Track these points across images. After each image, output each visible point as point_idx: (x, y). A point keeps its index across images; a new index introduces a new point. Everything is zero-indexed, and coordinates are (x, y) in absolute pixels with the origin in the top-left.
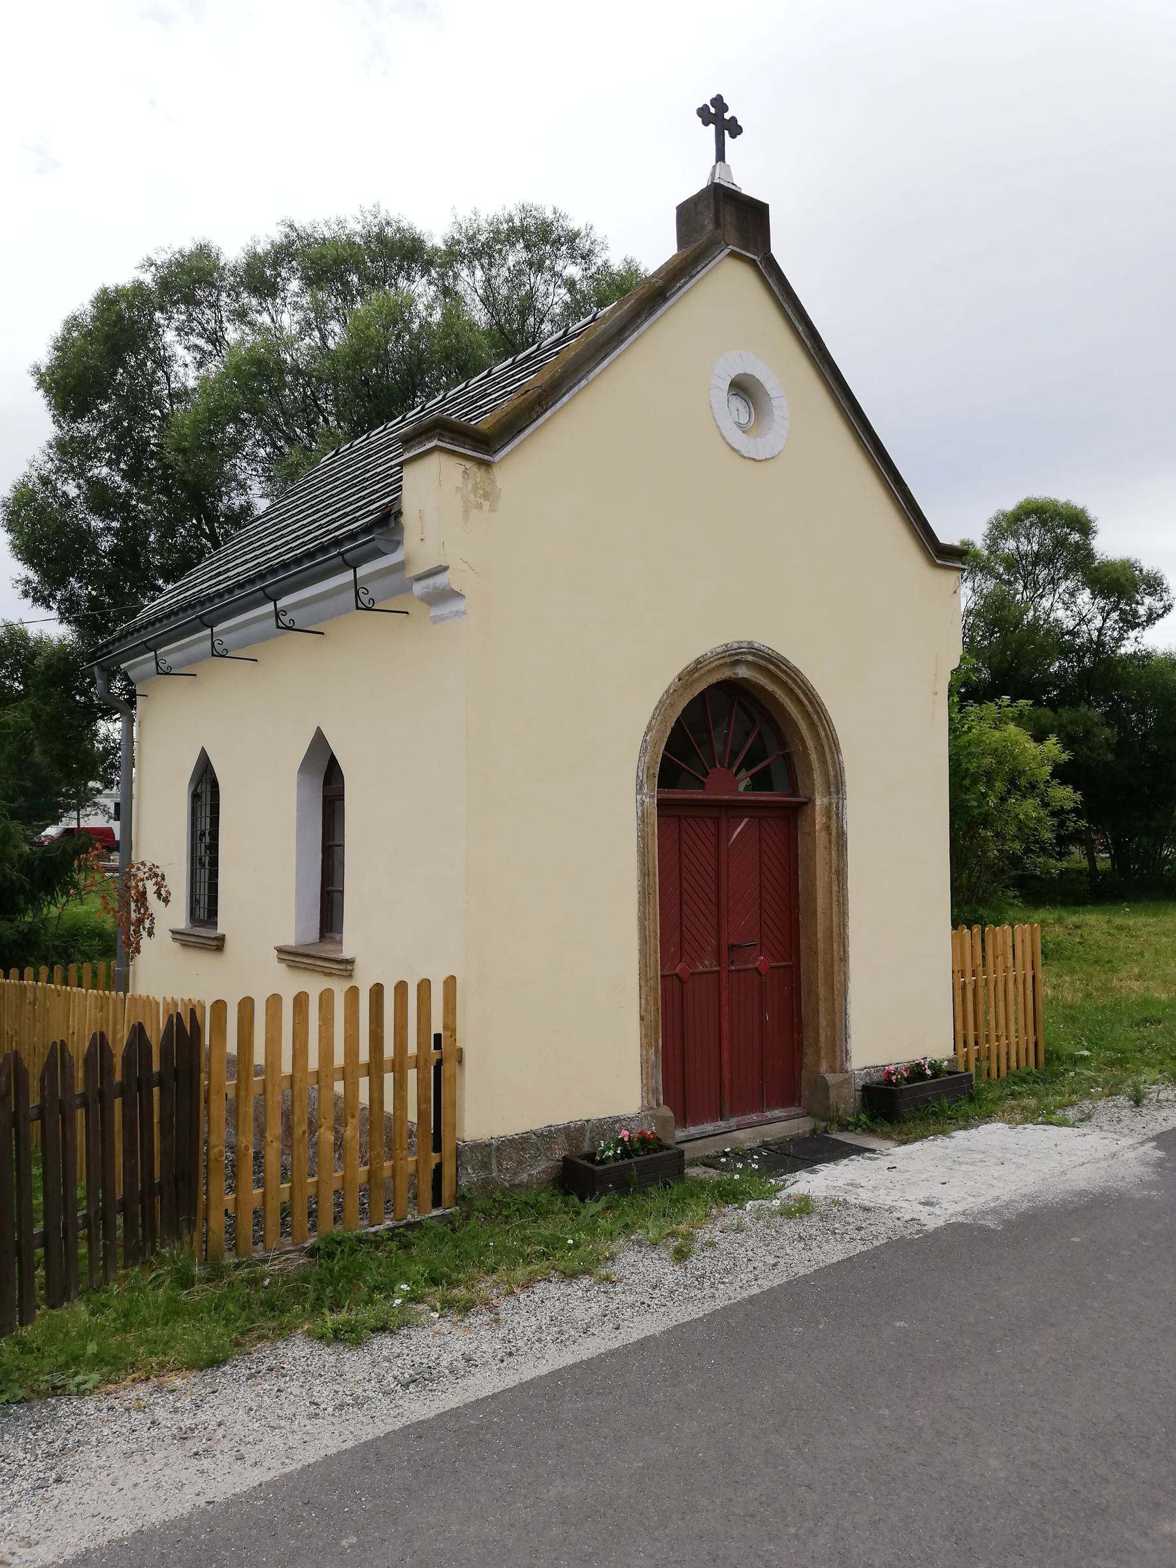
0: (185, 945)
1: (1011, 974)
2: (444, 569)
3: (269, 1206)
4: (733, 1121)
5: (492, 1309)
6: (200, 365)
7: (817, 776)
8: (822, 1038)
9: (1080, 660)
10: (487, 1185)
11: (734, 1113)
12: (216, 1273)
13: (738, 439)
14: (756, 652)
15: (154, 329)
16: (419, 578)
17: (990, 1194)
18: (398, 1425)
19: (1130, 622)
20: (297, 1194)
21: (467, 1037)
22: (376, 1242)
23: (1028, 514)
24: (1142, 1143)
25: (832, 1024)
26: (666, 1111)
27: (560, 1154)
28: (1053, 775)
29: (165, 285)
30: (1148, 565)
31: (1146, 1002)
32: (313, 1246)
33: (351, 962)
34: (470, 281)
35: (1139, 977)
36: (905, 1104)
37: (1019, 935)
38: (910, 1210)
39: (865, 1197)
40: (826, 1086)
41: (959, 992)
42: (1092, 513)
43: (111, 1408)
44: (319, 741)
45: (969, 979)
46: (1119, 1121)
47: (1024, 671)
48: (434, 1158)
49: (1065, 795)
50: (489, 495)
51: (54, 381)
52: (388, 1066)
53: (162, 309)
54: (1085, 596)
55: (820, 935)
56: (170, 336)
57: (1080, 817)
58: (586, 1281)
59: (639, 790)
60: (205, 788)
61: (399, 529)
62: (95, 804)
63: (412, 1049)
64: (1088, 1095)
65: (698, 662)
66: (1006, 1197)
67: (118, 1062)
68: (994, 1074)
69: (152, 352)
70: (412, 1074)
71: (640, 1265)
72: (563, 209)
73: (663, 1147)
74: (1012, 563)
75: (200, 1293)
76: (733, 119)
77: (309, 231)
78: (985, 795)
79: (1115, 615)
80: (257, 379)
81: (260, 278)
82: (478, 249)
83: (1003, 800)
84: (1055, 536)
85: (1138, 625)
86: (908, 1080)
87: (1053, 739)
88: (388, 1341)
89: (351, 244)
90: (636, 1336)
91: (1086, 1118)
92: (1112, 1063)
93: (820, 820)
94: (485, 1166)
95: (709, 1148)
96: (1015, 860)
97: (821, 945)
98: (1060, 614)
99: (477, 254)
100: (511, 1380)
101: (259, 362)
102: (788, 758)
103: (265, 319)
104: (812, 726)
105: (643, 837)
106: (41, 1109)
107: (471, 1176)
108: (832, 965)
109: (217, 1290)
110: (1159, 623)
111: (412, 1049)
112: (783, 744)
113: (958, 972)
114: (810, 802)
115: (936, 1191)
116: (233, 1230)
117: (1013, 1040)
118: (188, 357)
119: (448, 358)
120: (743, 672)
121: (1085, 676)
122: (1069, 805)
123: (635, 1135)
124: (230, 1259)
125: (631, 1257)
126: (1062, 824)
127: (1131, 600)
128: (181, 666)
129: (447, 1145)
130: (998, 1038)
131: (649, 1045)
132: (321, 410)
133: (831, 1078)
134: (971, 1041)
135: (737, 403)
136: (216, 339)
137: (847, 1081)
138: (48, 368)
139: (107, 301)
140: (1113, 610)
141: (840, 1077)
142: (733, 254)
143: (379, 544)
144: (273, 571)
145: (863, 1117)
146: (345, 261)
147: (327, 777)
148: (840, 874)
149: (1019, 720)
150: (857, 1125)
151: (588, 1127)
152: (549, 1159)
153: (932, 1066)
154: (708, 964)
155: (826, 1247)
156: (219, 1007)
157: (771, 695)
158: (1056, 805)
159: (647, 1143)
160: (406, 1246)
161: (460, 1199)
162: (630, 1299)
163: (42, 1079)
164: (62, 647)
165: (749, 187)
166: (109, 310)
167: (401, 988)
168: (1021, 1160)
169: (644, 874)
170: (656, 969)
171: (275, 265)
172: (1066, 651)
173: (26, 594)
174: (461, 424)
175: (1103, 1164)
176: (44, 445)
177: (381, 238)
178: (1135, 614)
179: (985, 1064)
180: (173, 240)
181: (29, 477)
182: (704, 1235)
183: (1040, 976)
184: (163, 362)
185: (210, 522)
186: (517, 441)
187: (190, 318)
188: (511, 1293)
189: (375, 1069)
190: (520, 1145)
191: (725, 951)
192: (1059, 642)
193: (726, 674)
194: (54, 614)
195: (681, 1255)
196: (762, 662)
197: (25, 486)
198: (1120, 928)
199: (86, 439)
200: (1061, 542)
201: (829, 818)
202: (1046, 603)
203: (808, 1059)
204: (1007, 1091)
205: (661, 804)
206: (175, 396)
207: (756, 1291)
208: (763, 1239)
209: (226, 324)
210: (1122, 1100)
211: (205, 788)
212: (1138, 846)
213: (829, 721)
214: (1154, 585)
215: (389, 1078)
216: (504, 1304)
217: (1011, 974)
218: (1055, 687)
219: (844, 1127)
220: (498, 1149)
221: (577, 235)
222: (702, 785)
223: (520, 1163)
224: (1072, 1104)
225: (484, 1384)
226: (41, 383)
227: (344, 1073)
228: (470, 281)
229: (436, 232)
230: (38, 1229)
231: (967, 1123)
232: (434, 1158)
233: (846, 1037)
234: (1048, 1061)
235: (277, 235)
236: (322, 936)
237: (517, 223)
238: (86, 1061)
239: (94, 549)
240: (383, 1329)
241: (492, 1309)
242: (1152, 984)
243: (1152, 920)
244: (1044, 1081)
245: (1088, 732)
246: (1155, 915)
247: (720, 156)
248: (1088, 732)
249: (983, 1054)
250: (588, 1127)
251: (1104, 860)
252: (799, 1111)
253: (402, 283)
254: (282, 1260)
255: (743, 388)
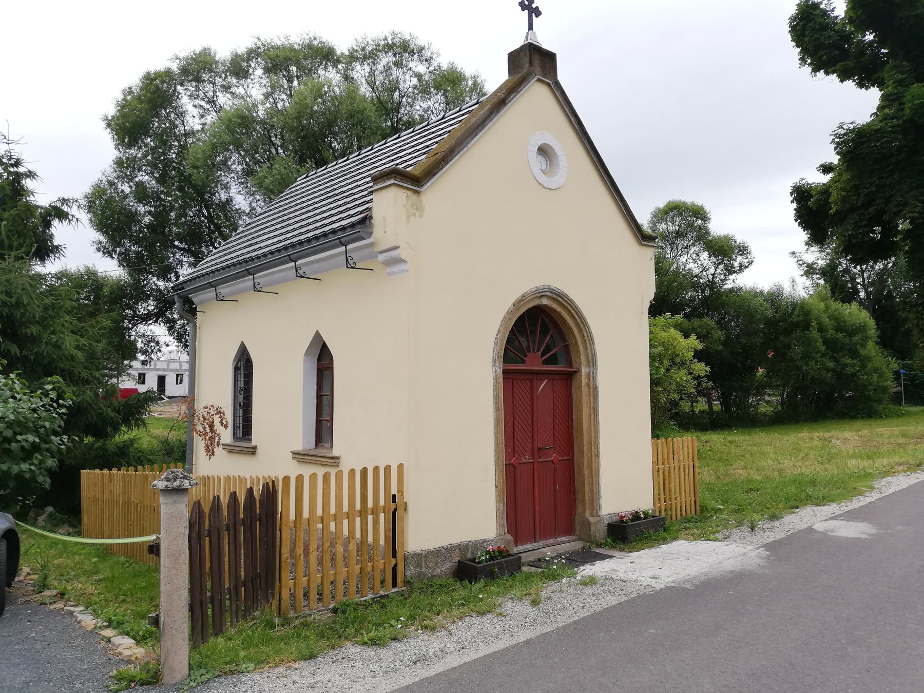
0: (230, 452)
1: (682, 464)
2: (397, 248)
3: (311, 586)
4: (541, 543)
5: (447, 629)
6: (202, 116)
7: (583, 357)
8: (587, 498)
9: (703, 291)
10: (420, 575)
11: (544, 536)
12: (286, 622)
13: (542, 178)
14: (552, 291)
15: (175, 96)
16: (382, 252)
17: (685, 573)
18: (417, 680)
19: (730, 270)
20: (325, 579)
21: (409, 497)
22: (367, 605)
23: (672, 210)
24: (758, 548)
25: (592, 490)
26: (509, 537)
27: (456, 559)
28: (694, 357)
29: (185, 71)
30: (739, 239)
31: (750, 481)
32: (334, 608)
33: (337, 458)
34: (360, 72)
35: (744, 468)
36: (628, 533)
37: (685, 443)
38: (646, 581)
39: (621, 575)
40: (590, 524)
41: (656, 474)
42: (707, 208)
43: (268, 677)
44: (318, 337)
45: (661, 466)
46: (745, 538)
47: (672, 297)
48: (393, 561)
49: (701, 368)
50: (419, 208)
51: (117, 125)
52: (370, 512)
53: (182, 85)
54: (705, 255)
55: (585, 443)
56: (185, 100)
57: (709, 380)
58: (490, 616)
59: (494, 365)
60: (244, 365)
61: (371, 226)
62: (128, 374)
63: (382, 503)
64: (725, 527)
65: (523, 296)
66: (693, 574)
67: (242, 506)
68: (674, 518)
69: (175, 108)
70: (382, 516)
71: (515, 608)
72: (415, 34)
73: (510, 555)
74: (665, 237)
75: (279, 632)
76: (537, 7)
77: (269, 41)
78: (658, 367)
79: (721, 267)
80: (240, 128)
81: (238, 68)
82: (365, 55)
83: (668, 370)
84: (687, 221)
85: (734, 272)
86: (632, 520)
87: (694, 337)
88: (398, 645)
89: (292, 49)
90: (522, 639)
91: (727, 538)
92: (735, 511)
93: (584, 381)
94: (419, 565)
95: (532, 557)
96: (675, 404)
97: (585, 448)
98: (691, 265)
99: (365, 58)
100: (466, 659)
101: (243, 117)
102: (567, 347)
103: (240, 91)
104: (580, 330)
105: (496, 390)
106: (209, 531)
107: (412, 571)
108: (591, 459)
109: (285, 630)
110: (746, 271)
111: (382, 503)
112: (564, 339)
113: (656, 462)
114: (578, 371)
115: (657, 572)
116: (293, 596)
117: (684, 500)
118: (195, 112)
119: (352, 116)
120: (545, 301)
121: (705, 300)
122: (703, 374)
123: (495, 548)
124: (292, 614)
125: (509, 605)
126: (699, 384)
127: (730, 259)
128: (228, 296)
129: (400, 555)
130: (676, 499)
131: (500, 501)
132: (273, 144)
133: (592, 520)
134: (662, 500)
135: (541, 159)
136: (212, 102)
137: (600, 521)
138: (113, 117)
139: (150, 79)
140: (720, 264)
141: (596, 519)
142: (539, 80)
143: (361, 234)
144: (293, 245)
145: (609, 540)
146: (290, 59)
147: (322, 359)
148: (595, 410)
149: (676, 326)
150: (606, 545)
151: (470, 545)
152: (451, 562)
153: (644, 513)
154: (527, 458)
155: (607, 599)
156: (287, 479)
157: (559, 314)
158: (696, 373)
159: (502, 553)
160: (383, 606)
161: (407, 583)
162: (515, 623)
163: (210, 516)
164: (119, 281)
165: (546, 45)
166: (150, 84)
167: (376, 469)
168: (698, 557)
169: (497, 409)
170: (503, 461)
171: (249, 60)
172: (695, 286)
173: (98, 250)
174: (407, 172)
175: (740, 558)
176: (111, 162)
177: (310, 46)
178: (732, 267)
179: (669, 513)
180: (188, 46)
181: (101, 181)
182: (544, 594)
183: (697, 465)
184: (182, 115)
185: (207, 208)
186: (433, 180)
187: (197, 89)
188: (454, 622)
189: (363, 513)
190: (437, 554)
191: (536, 451)
192: (692, 282)
193: (536, 302)
194: (115, 262)
195: (535, 603)
196: (555, 296)
197: (99, 187)
198: (731, 442)
199: (134, 159)
200: (691, 225)
201: (589, 379)
202: (683, 259)
203: (579, 509)
204: (682, 526)
205: (507, 374)
206: (186, 135)
207: (577, 618)
208: (575, 595)
209: (218, 93)
210: (744, 528)
211: (244, 365)
212: (736, 397)
213: (588, 328)
214: (743, 250)
215: (370, 518)
216: (452, 627)
217: (682, 464)
218: (689, 306)
219: (599, 546)
220: (425, 556)
221: (423, 48)
222: (523, 362)
223: (436, 564)
224: (718, 532)
225: (454, 661)
226: (109, 125)
227: (322, 519)
228: (360, 72)
229: (342, 47)
230: (209, 594)
231: (665, 541)
232: (393, 561)
233: (599, 497)
234: (702, 511)
235: (250, 43)
236: (317, 445)
237: (390, 41)
238: (228, 506)
239: (140, 222)
240: (394, 639)
241: (447, 629)
242: (752, 472)
243: (747, 438)
244: (700, 521)
245: (708, 333)
246: (749, 435)
247: (531, 27)
248: (708, 333)
249: (668, 506)
250: (470, 545)
251: (717, 406)
252: (575, 537)
253: (321, 72)
254: (320, 615)
255: (543, 151)
